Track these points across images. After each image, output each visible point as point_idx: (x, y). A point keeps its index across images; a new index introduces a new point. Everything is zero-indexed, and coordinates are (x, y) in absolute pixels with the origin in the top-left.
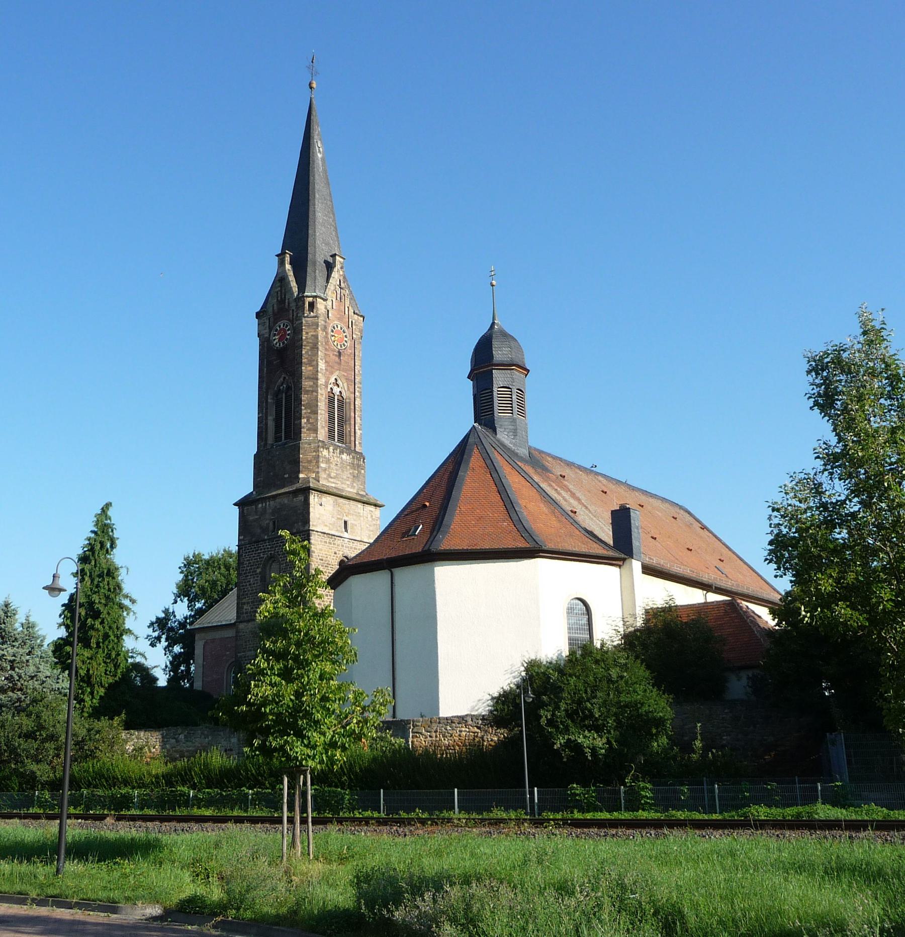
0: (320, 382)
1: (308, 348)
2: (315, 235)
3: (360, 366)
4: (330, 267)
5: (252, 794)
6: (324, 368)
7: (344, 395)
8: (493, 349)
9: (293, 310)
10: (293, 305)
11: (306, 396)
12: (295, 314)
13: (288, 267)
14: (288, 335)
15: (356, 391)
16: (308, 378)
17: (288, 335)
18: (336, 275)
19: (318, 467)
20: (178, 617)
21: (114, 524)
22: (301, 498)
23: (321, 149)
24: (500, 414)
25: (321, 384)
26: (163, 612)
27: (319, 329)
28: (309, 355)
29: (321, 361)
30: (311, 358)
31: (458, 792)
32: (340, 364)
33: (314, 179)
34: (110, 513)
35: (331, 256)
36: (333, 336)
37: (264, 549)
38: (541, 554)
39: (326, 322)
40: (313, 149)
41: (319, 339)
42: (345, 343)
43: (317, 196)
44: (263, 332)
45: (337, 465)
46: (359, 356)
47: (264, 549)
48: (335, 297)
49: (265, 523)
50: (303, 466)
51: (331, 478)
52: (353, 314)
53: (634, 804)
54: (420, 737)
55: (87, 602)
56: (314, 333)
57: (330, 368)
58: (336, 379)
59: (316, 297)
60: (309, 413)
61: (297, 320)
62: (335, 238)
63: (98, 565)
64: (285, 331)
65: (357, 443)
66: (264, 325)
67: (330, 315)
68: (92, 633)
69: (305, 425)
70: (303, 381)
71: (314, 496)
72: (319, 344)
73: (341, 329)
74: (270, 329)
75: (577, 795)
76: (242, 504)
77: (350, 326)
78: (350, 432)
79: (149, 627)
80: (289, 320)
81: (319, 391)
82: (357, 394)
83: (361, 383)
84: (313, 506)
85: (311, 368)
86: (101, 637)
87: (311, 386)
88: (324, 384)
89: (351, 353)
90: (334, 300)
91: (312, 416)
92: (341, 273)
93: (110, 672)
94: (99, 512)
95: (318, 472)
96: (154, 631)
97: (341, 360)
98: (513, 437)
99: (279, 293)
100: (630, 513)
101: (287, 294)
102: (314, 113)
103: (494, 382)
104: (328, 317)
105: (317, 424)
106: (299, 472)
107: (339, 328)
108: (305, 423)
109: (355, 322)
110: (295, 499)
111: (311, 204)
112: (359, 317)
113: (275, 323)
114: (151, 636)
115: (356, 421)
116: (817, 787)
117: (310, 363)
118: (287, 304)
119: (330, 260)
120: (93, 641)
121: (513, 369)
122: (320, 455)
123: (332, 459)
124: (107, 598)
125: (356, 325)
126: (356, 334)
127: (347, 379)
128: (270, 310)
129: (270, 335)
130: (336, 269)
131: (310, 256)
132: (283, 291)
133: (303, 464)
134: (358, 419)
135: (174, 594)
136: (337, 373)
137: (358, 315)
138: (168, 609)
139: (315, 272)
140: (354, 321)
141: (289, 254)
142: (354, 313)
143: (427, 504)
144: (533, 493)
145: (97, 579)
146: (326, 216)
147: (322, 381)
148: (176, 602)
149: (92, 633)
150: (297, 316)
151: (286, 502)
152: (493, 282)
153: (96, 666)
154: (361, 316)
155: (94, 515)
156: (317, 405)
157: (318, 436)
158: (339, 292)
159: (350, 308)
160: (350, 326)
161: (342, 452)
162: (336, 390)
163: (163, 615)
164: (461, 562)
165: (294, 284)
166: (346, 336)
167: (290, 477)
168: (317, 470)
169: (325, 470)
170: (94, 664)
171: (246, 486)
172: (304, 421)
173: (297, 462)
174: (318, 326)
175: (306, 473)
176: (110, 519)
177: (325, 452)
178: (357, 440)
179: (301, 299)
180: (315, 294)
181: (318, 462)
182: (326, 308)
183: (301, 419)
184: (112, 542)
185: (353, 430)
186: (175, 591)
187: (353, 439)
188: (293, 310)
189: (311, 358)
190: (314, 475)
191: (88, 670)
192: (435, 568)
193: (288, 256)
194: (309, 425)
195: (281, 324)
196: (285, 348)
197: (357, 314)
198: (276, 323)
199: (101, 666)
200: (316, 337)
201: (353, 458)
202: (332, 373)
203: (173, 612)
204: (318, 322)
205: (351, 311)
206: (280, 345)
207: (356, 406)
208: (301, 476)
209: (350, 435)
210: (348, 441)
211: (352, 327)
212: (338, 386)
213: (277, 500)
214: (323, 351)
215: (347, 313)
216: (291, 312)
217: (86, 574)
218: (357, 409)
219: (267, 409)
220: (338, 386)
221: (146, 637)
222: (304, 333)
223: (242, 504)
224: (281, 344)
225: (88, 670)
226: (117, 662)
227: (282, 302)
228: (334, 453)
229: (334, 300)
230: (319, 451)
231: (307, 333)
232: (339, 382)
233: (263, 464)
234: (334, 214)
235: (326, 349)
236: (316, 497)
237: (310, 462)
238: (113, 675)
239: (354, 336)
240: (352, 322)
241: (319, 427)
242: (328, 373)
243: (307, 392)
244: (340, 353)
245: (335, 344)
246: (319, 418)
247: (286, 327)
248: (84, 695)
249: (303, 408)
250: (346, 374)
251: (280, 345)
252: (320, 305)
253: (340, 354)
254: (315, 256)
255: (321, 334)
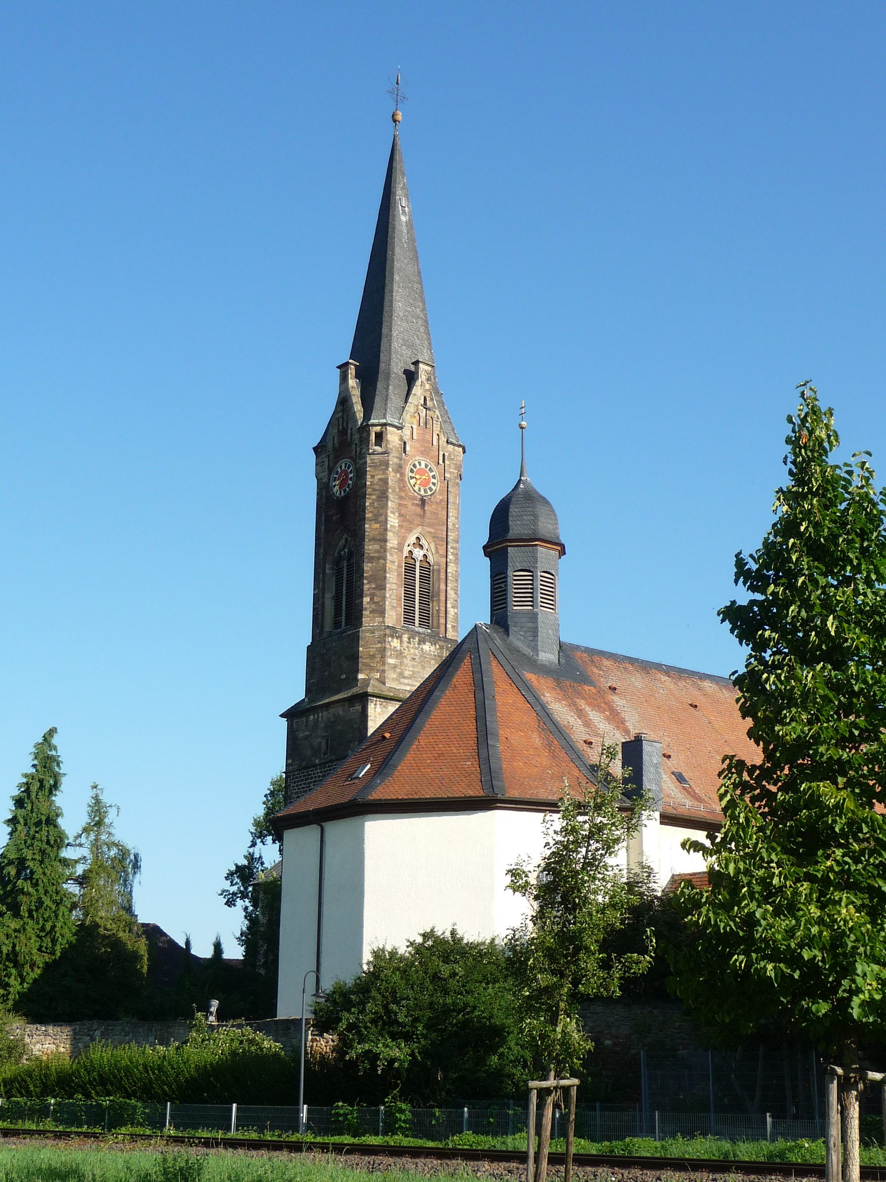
0: (389, 545)
1: (374, 497)
2: (391, 336)
3: (457, 518)
4: (411, 377)
5: (55, 1104)
6: (397, 525)
7: (431, 559)
8: (510, 518)
9: (356, 444)
10: (356, 437)
11: (370, 565)
12: (358, 449)
13: (352, 382)
14: (351, 479)
15: (449, 553)
16: (373, 539)
17: (351, 479)
18: (418, 391)
19: (384, 664)
20: (267, 865)
21: (59, 756)
22: (358, 707)
23: (407, 209)
24: (515, 608)
25: (391, 548)
26: (245, 857)
27: (390, 469)
28: (375, 508)
29: (392, 515)
30: (378, 512)
31: (237, 1108)
32: (423, 516)
33: (393, 254)
34: (55, 741)
35: (413, 364)
36: (412, 478)
37: (315, 778)
38: (498, 805)
39: (401, 459)
40: (394, 211)
41: (390, 484)
42: (432, 486)
43: (396, 278)
44: (321, 475)
45: (414, 659)
46: (454, 503)
47: (315, 778)
48: (415, 421)
49: (316, 741)
50: (363, 664)
51: (405, 677)
52: (445, 444)
53: (390, 1129)
54: (320, 1041)
55: (18, 858)
56: (383, 477)
57: (407, 524)
58: (418, 538)
59: (385, 425)
60: (374, 589)
61: (360, 459)
62: (425, 336)
63: (36, 810)
64: (347, 475)
65: (449, 626)
66: (322, 466)
67: (408, 448)
68: (21, 898)
69: (368, 606)
70: (366, 543)
71: (375, 704)
72: (390, 490)
73: (426, 466)
74: (330, 470)
75: (341, 1115)
76: (290, 715)
77: (441, 462)
78: (438, 611)
79: (227, 878)
80: (351, 458)
81: (389, 557)
82: (450, 557)
83: (457, 542)
84: (372, 718)
85: (377, 526)
86: (33, 904)
87: (377, 551)
88: (396, 546)
89: (441, 500)
90: (415, 427)
91: (377, 592)
92: (427, 387)
93: (46, 948)
94: (41, 741)
95: (383, 671)
96: (232, 885)
97: (424, 510)
98: (531, 639)
99: (341, 420)
100: (642, 746)
101: (350, 422)
102: (397, 157)
103: (510, 564)
104: (405, 451)
105: (385, 603)
106: (357, 671)
107: (423, 466)
108: (368, 603)
109: (449, 455)
110: (351, 709)
111: (387, 289)
112: (456, 448)
113: (336, 463)
114: (227, 891)
115: (448, 596)
116: (463, 1112)
117: (376, 519)
118: (349, 435)
119: (412, 368)
120: (24, 909)
121: (536, 545)
122: (388, 646)
123: (406, 651)
124: (43, 852)
125: (450, 459)
126: (450, 473)
127: (434, 537)
128: (330, 445)
129: (329, 480)
130: (418, 383)
131: (382, 366)
132: (345, 417)
133: (364, 661)
134: (451, 593)
135: (252, 833)
136: (419, 529)
137: (454, 445)
138: (253, 853)
139: (387, 389)
140: (446, 454)
141: (355, 365)
142: (447, 442)
143: (387, 735)
144: (530, 718)
145: (33, 829)
146: (411, 305)
147: (392, 541)
148: (254, 844)
149: (21, 898)
150: (360, 453)
151: (341, 713)
152: (523, 423)
153: (25, 941)
154: (460, 446)
155: (34, 745)
156: (385, 578)
157: (386, 620)
158: (423, 415)
159: (442, 436)
160: (441, 462)
161: (422, 641)
162: (418, 554)
163: (246, 863)
164: (399, 815)
165: (358, 408)
166: (434, 477)
167: (347, 678)
168: (382, 668)
169: (395, 667)
170: (23, 937)
171: (297, 693)
172: (366, 599)
173: (354, 657)
174: (387, 464)
175: (367, 672)
176: (55, 749)
177: (395, 643)
178: (448, 622)
179: (365, 429)
180: (384, 421)
181: (383, 657)
182: (401, 439)
183: (362, 597)
184: (56, 779)
185: (443, 609)
186: (253, 830)
187: (442, 621)
188: (356, 444)
189: (378, 512)
190: (378, 675)
191: (14, 946)
192: (366, 823)
193: (352, 367)
194: (373, 606)
195: (343, 464)
196: (346, 498)
197: (452, 444)
198: (337, 462)
199: (32, 941)
200: (385, 481)
201: (441, 648)
202: (410, 530)
203: (260, 857)
204: (388, 461)
205: (443, 439)
206: (340, 494)
207: (449, 575)
208: (361, 676)
209: (439, 616)
210: (435, 625)
211: (444, 462)
212: (421, 547)
213: (332, 711)
214: (397, 501)
215: (435, 443)
216: (354, 446)
217: (18, 822)
218: (450, 578)
219: (324, 582)
220: (421, 547)
221: (220, 892)
222: (368, 477)
223: (290, 715)
224: (342, 492)
225: (14, 946)
226: (55, 936)
227: (343, 432)
228: (409, 642)
229: (415, 427)
230: (385, 641)
231: (373, 477)
232: (423, 542)
233: (317, 660)
234: (423, 302)
235: (401, 498)
236: (378, 706)
237: (372, 657)
238: (50, 953)
239: (447, 475)
240: (444, 455)
241: (387, 608)
242: (403, 531)
243: (371, 559)
244: (423, 502)
245: (416, 488)
246: (387, 595)
247: (348, 469)
248: (9, 978)
249: (365, 581)
250: (432, 530)
251: (340, 494)
252: (393, 437)
253: (423, 502)
254: (389, 365)
255: (392, 477)
